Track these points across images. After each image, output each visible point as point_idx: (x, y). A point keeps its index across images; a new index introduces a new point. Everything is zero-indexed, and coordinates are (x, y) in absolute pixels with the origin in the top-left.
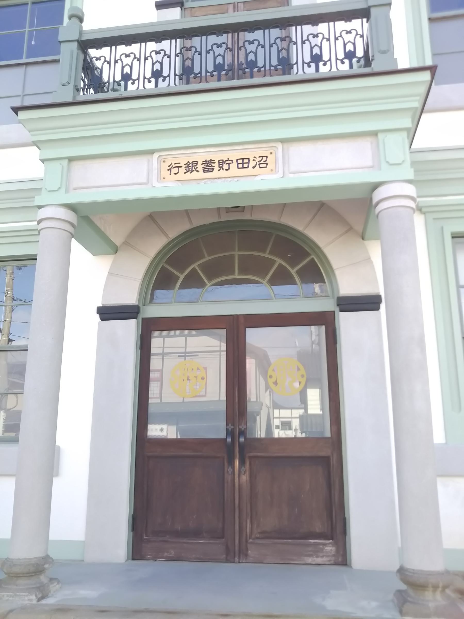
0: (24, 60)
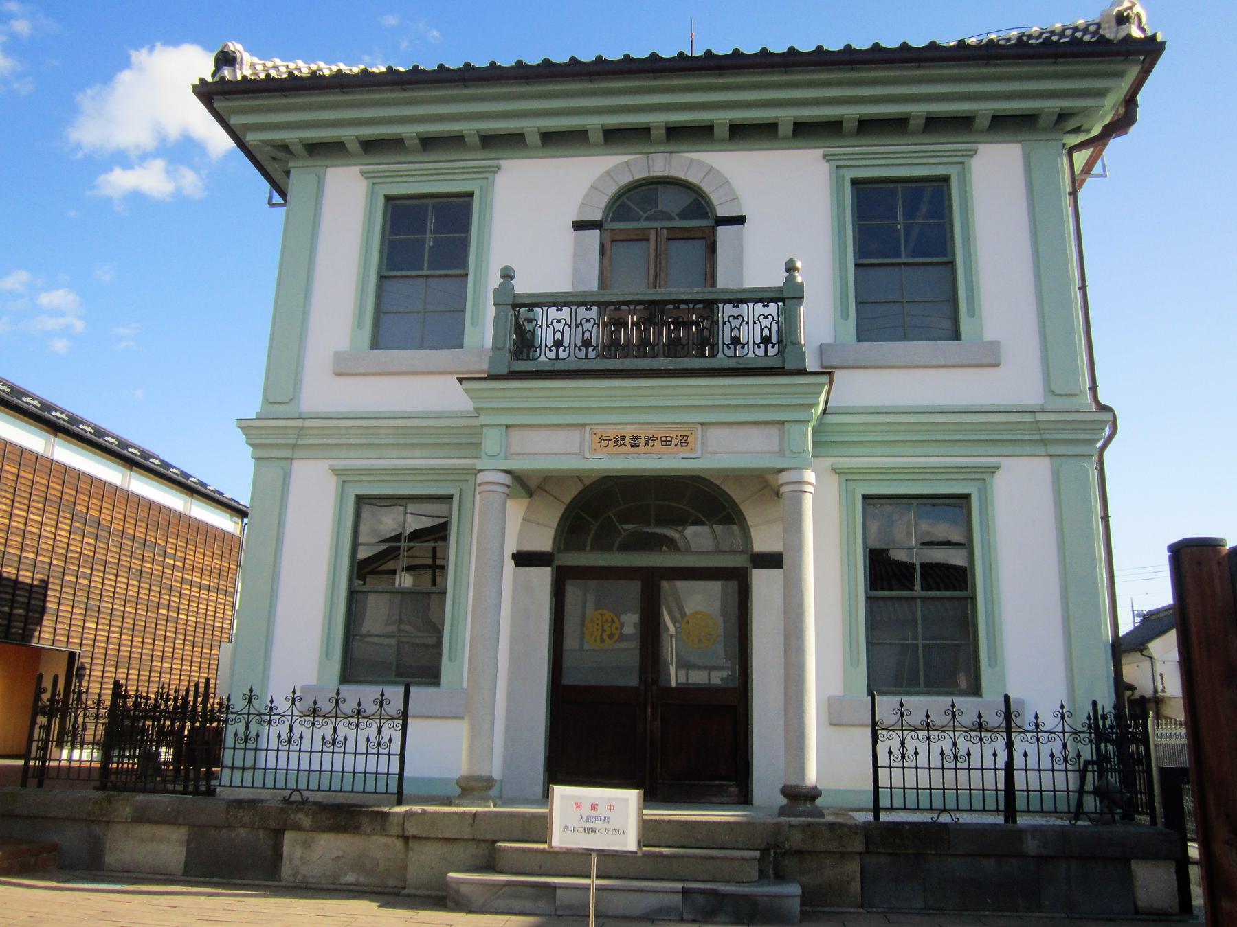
0: (425, 272)
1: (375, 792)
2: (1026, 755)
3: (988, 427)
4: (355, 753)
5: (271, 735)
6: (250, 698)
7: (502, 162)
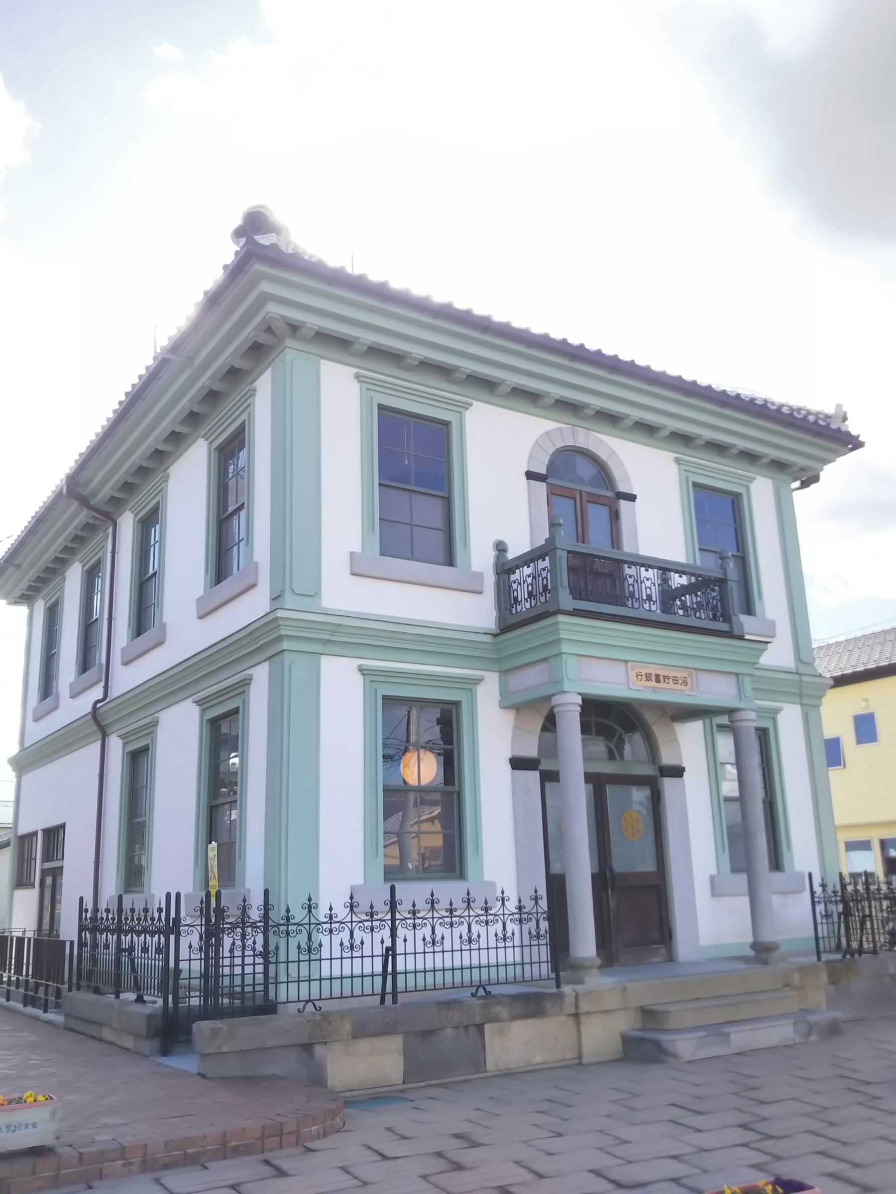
1: (532, 980)
2: (405, 940)
3: (382, 634)
4: (488, 949)
5: (329, 945)
6: (310, 907)
7: (475, 402)
